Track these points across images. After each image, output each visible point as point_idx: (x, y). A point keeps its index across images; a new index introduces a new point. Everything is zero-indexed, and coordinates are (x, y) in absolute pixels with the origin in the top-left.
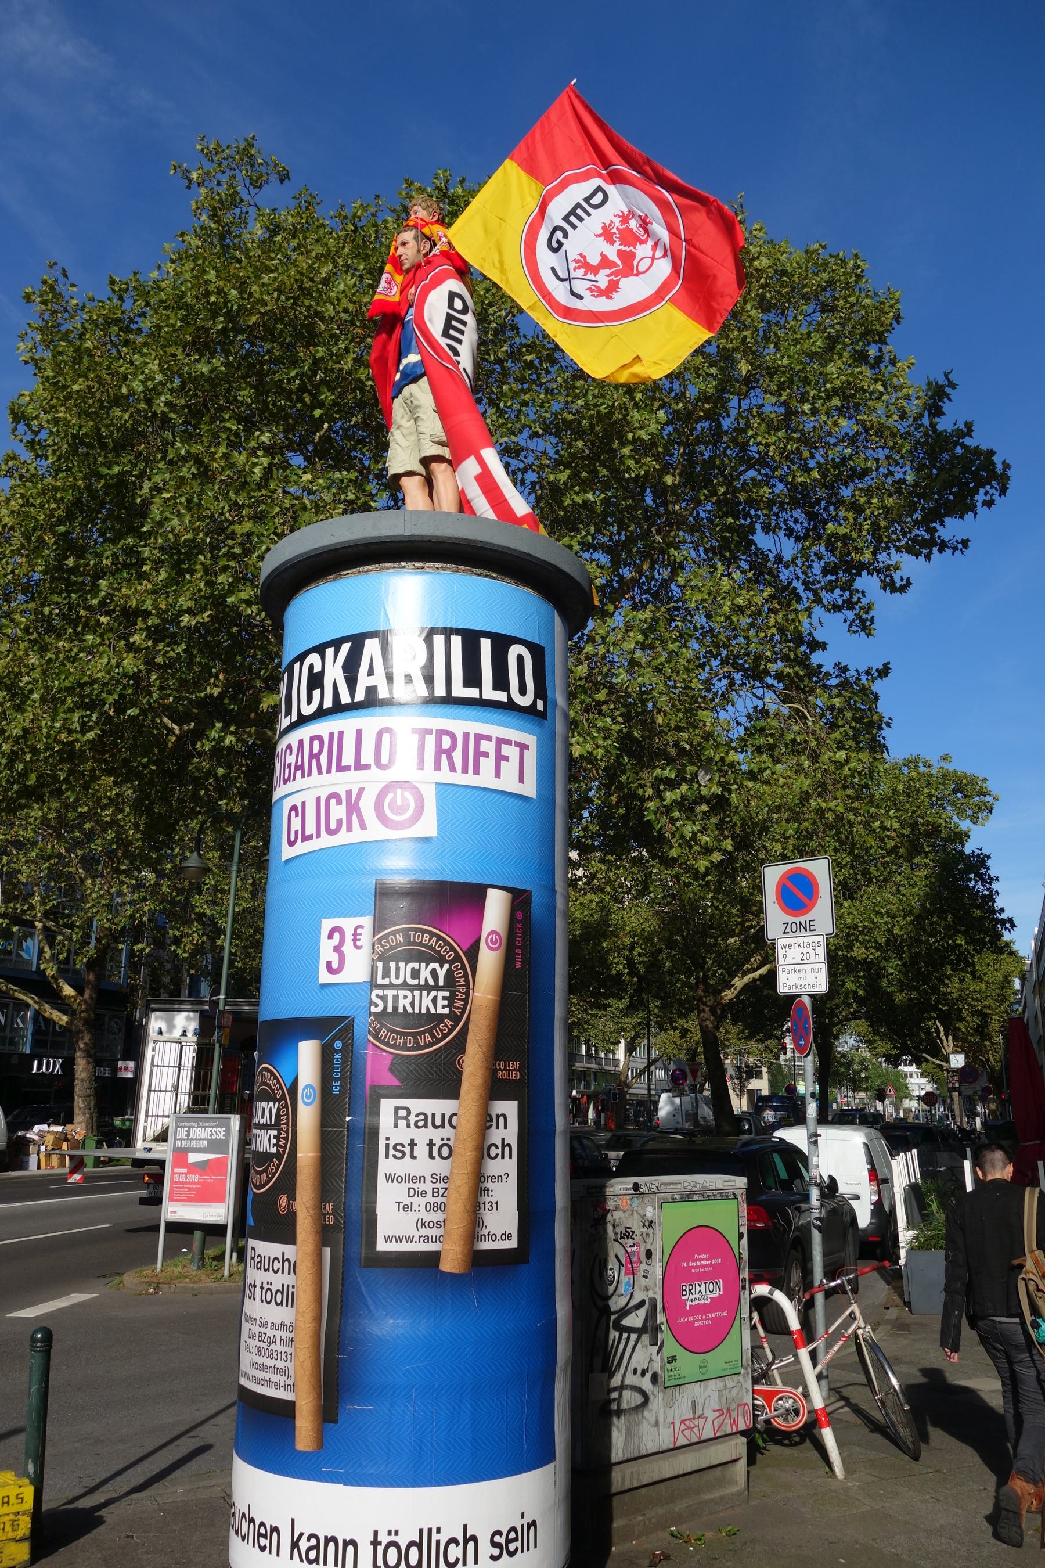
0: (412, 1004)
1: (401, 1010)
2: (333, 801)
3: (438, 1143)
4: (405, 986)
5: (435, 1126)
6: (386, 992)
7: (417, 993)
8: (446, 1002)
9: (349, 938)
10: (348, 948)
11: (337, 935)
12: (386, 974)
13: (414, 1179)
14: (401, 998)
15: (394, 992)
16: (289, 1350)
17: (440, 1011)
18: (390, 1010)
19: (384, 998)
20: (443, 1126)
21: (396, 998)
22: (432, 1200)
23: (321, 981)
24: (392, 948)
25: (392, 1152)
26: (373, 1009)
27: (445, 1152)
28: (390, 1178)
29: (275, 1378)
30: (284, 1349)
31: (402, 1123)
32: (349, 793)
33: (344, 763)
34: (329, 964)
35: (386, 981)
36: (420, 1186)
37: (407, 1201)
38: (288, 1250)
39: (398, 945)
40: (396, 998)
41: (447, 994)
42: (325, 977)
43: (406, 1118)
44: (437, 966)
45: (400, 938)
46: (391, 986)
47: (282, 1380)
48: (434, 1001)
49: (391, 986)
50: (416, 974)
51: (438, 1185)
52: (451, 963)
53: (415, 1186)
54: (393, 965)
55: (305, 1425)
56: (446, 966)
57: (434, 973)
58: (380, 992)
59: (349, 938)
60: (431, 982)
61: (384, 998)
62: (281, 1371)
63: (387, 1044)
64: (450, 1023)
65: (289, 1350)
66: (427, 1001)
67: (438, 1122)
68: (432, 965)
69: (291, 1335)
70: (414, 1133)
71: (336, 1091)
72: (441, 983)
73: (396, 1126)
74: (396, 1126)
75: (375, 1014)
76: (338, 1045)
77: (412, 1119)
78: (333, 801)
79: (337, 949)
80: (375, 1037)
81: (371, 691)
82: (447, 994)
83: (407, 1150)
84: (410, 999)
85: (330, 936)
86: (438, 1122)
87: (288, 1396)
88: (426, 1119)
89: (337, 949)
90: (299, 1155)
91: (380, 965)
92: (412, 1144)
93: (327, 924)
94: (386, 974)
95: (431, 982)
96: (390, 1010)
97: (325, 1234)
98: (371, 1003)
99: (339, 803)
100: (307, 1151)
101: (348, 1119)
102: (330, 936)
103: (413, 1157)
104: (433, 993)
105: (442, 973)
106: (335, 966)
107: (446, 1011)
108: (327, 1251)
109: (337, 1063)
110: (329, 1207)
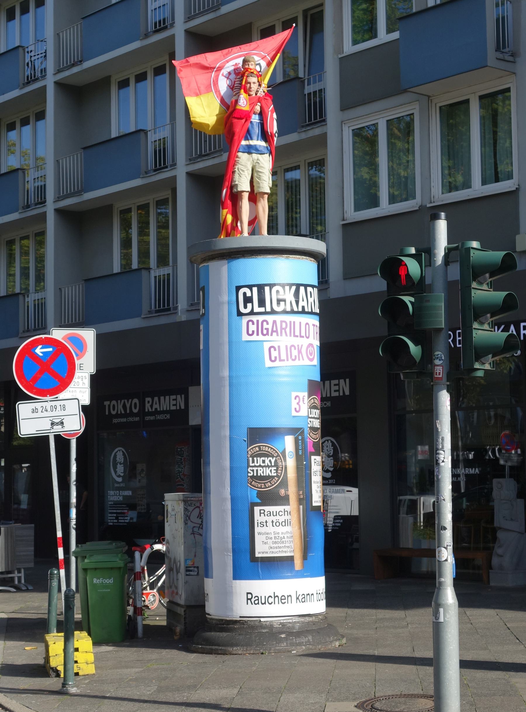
0: (263, 472)
1: (259, 475)
2: (293, 348)
3: (275, 521)
4: (260, 466)
5: (273, 515)
6: (254, 468)
7: (265, 468)
8: (275, 471)
9: (301, 400)
10: (301, 403)
11: (297, 398)
12: (253, 462)
13: (268, 534)
14: (259, 471)
15: (256, 468)
16: (291, 540)
17: (273, 474)
18: (255, 475)
19: (253, 471)
20: (276, 515)
21: (257, 470)
22: (274, 540)
23: (293, 415)
24: (255, 452)
25: (259, 525)
26: (249, 475)
27: (278, 524)
28: (259, 534)
29: (284, 550)
30: (288, 540)
31: (262, 515)
32: (298, 346)
33: (296, 334)
34: (295, 409)
35: (253, 465)
36: (270, 536)
37: (266, 541)
38: (287, 508)
39: (257, 452)
40: (257, 470)
41: (275, 468)
42: (294, 413)
43: (264, 513)
44: (271, 458)
45: (257, 449)
46: (255, 466)
47: (289, 550)
48: (271, 471)
49: (255, 466)
50: (264, 462)
51: (276, 535)
52: (276, 457)
53: (268, 536)
54: (255, 459)
55: (298, 563)
56: (275, 458)
57: (270, 461)
58: (251, 469)
59: (301, 400)
60: (269, 465)
61: (253, 471)
62: (288, 547)
63: (255, 487)
64: (277, 479)
65: (291, 540)
66: (268, 471)
67: (275, 514)
68: (269, 458)
69: (291, 535)
70: (266, 518)
71: (300, 453)
72: (273, 464)
73: (260, 516)
74: (260, 516)
75: (250, 477)
76: (300, 438)
77: (266, 513)
78: (293, 348)
79: (298, 403)
80: (251, 484)
81: (303, 307)
82: (275, 468)
83: (265, 524)
84: (262, 471)
85: (295, 399)
86: (275, 514)
87: (292, 554)
88: (270, 513)
89: (298, 403)
90: (288, 476)
91: (251, 459)
92: (266, 522)
93: (294, 394)
94: (253, 462)
95: (269, 465)
96: (255, 475)
97: (300, 501)
98: (248, 472)
99: (295, 349)
100: (291, 474)
101: (305, 463)
102: (295, 399)
103: (267, 526)
104: (270, 468)
105: (273, 461)
106: (298, 409)
107: (275, 474)
108: (301, 507)
109: (300, 444)
110: (301, 492)
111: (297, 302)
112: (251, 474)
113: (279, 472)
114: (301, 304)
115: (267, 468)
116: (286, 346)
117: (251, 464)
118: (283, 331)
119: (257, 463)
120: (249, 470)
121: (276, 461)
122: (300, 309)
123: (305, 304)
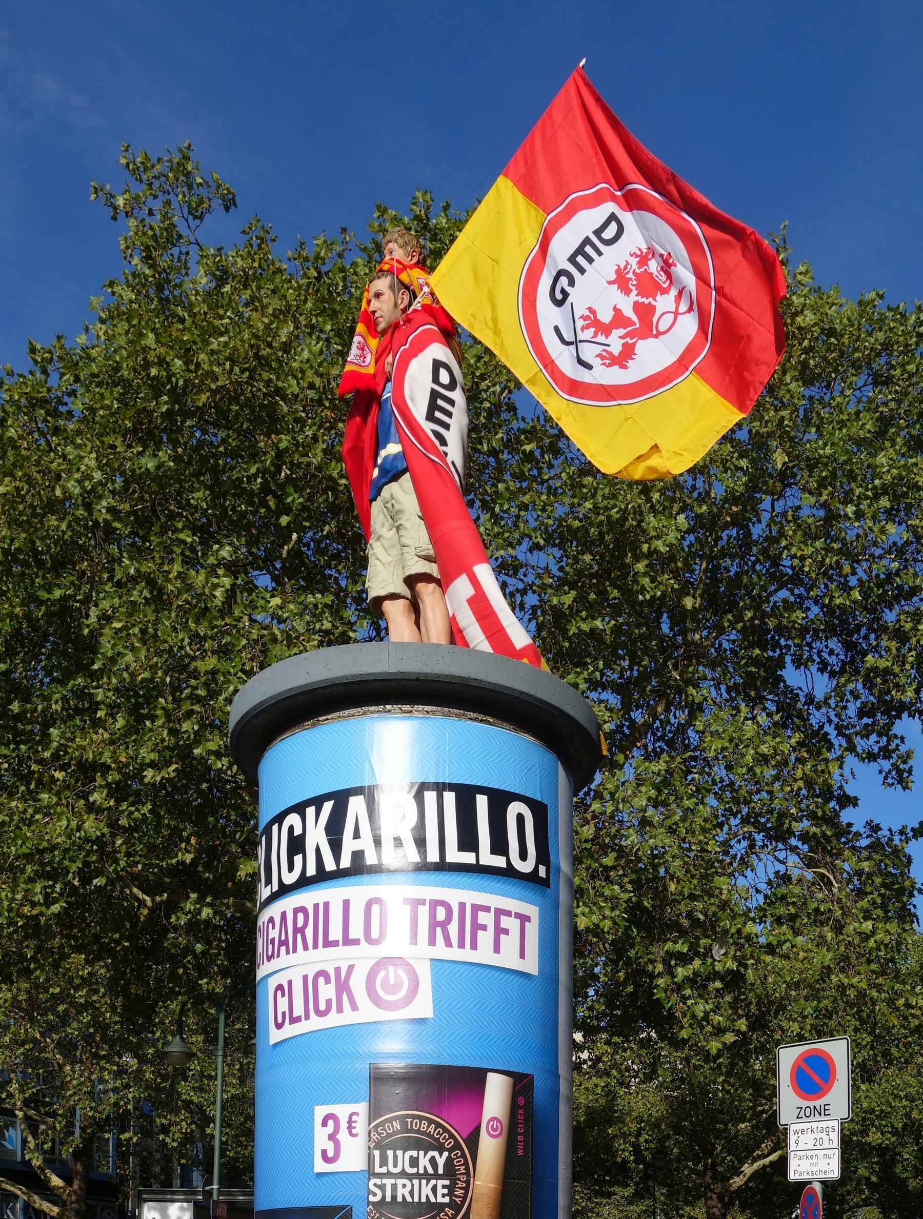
0: (411, 1193)
1: (400, 1199)
2: (321, 980)
7: (416, 1182)
8: (446, 1191)
9: (344, 1125)
10: (343, 1135)
11: (331, 1123)
12: (384, 1162)
15: (393, 1181)
17: (440, 1200)
19: (382, 1187)
21: (394, 1187)
26: (371, 1198)
32: (338, 970)
34: (324, 1153)
35: (384, 1170)
39: (394, 1133)
40: (394, 1187)
41: (447, 1182)
42: (320, 1166)
44: (436, 1154)
45: (397, 1125)
46: (389, 1175)
48: (434, 1189)
49: (389, 1175)
50: (414, 1162)
54: (390, 1153)
56: (446, 1154)
57: (433, 1161)
58: (378, 1181)
59: (344, 1125)
60: (431, 1171)
61: (382, 1187)
66: (427, 1190)
68: (431, 1153)
72: (441, 1171)
75: (374, 1204)
78: (321, 980)
79: (332, 1137)
81: (358, 856)
82: (447, 1182)
84: (409, 1187)
85: (324, 1124)
89: (332, 1137)
93: (320, 1112)
94: (384, 1162)
95: (431, 1171)
98: (370, 1192)
99: (328, 981)
102: (324, 1124)
104: (433, 1182)
105: (441, 1161)
106: (330, 1154)
107: (447, 1200)
111: (336, 847)
112: (378, 1198)
113: (459, 1192)
114: (349, 845)
115: (424, 1182)
116: (305, 978)
117: (378, 1170)
118: (299, 935)
119: (395, 1166)
120: (372, 1188)
121: (449, 1161)
122: (346, 863)
123: (365, 843)
